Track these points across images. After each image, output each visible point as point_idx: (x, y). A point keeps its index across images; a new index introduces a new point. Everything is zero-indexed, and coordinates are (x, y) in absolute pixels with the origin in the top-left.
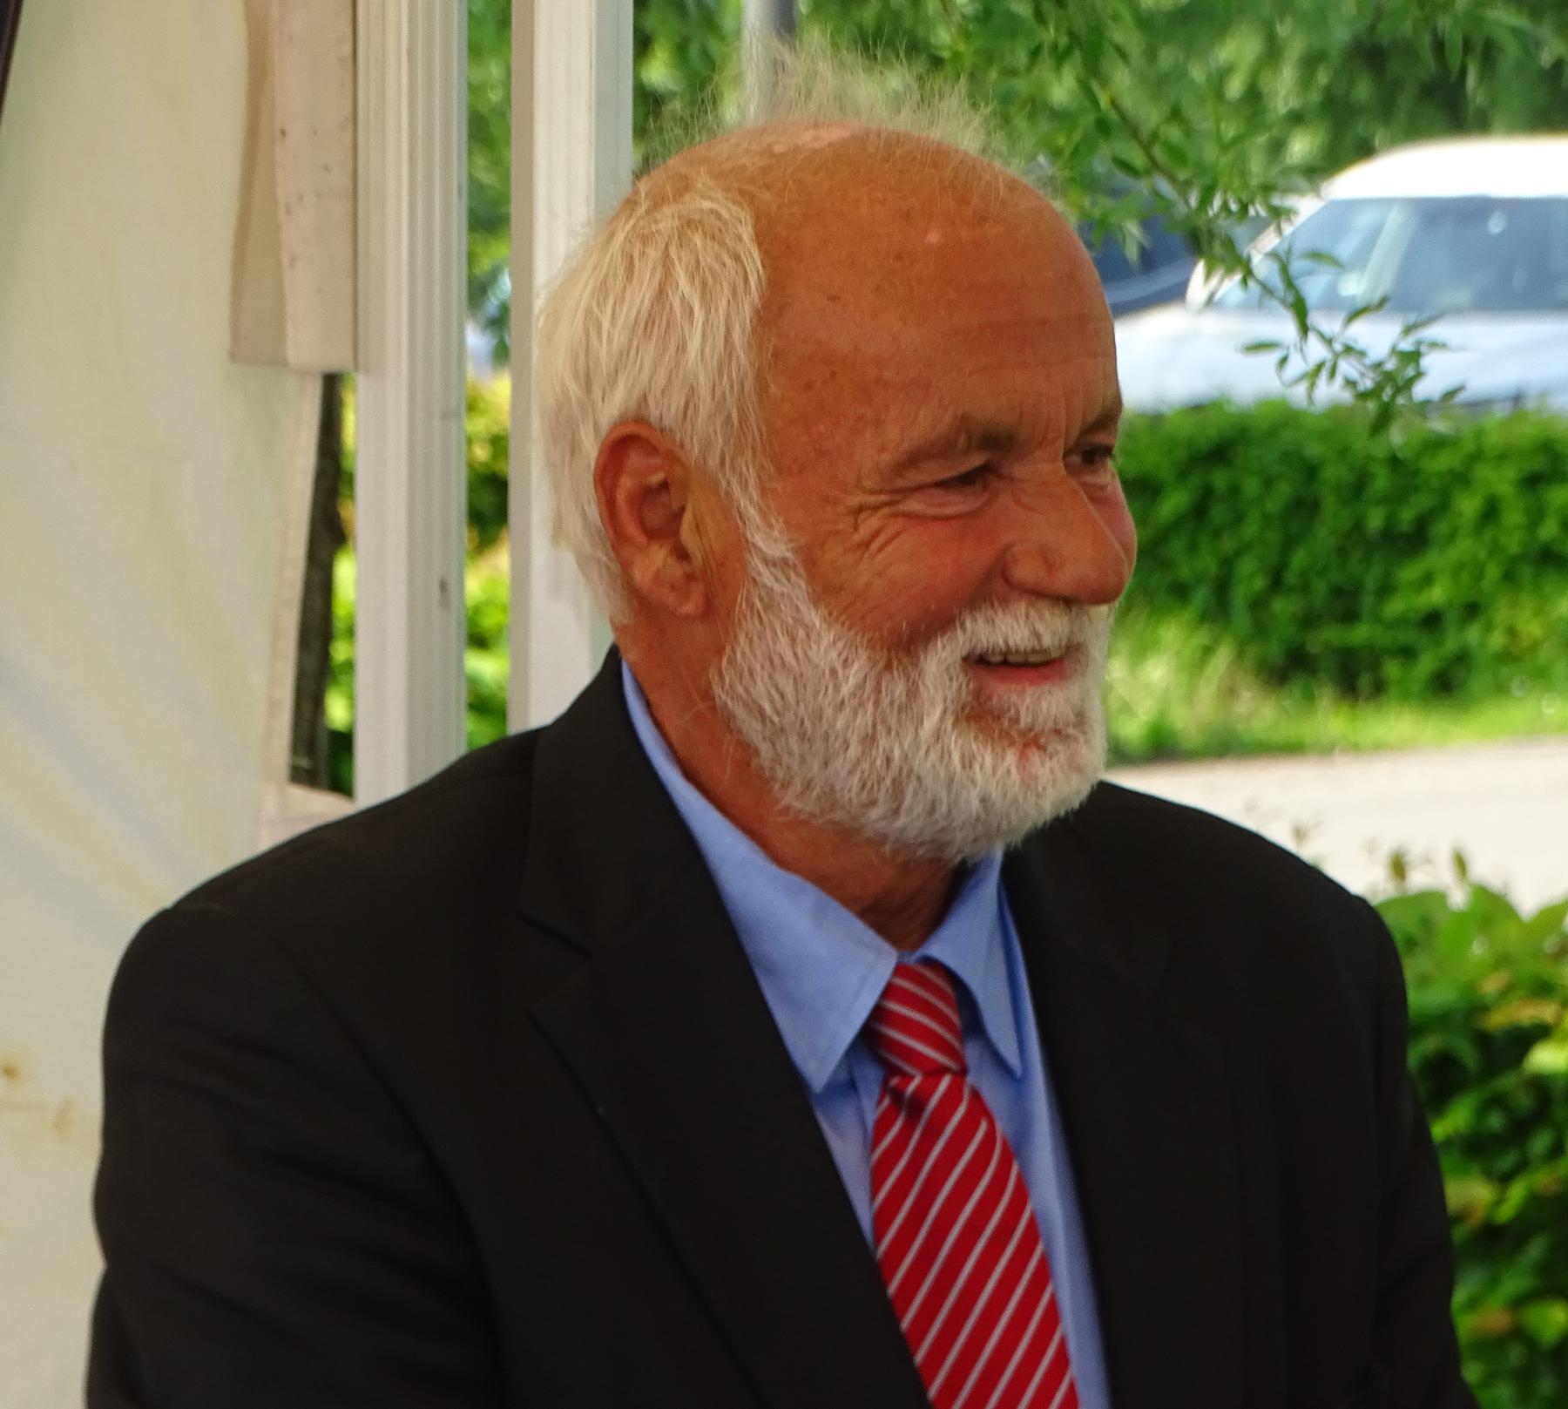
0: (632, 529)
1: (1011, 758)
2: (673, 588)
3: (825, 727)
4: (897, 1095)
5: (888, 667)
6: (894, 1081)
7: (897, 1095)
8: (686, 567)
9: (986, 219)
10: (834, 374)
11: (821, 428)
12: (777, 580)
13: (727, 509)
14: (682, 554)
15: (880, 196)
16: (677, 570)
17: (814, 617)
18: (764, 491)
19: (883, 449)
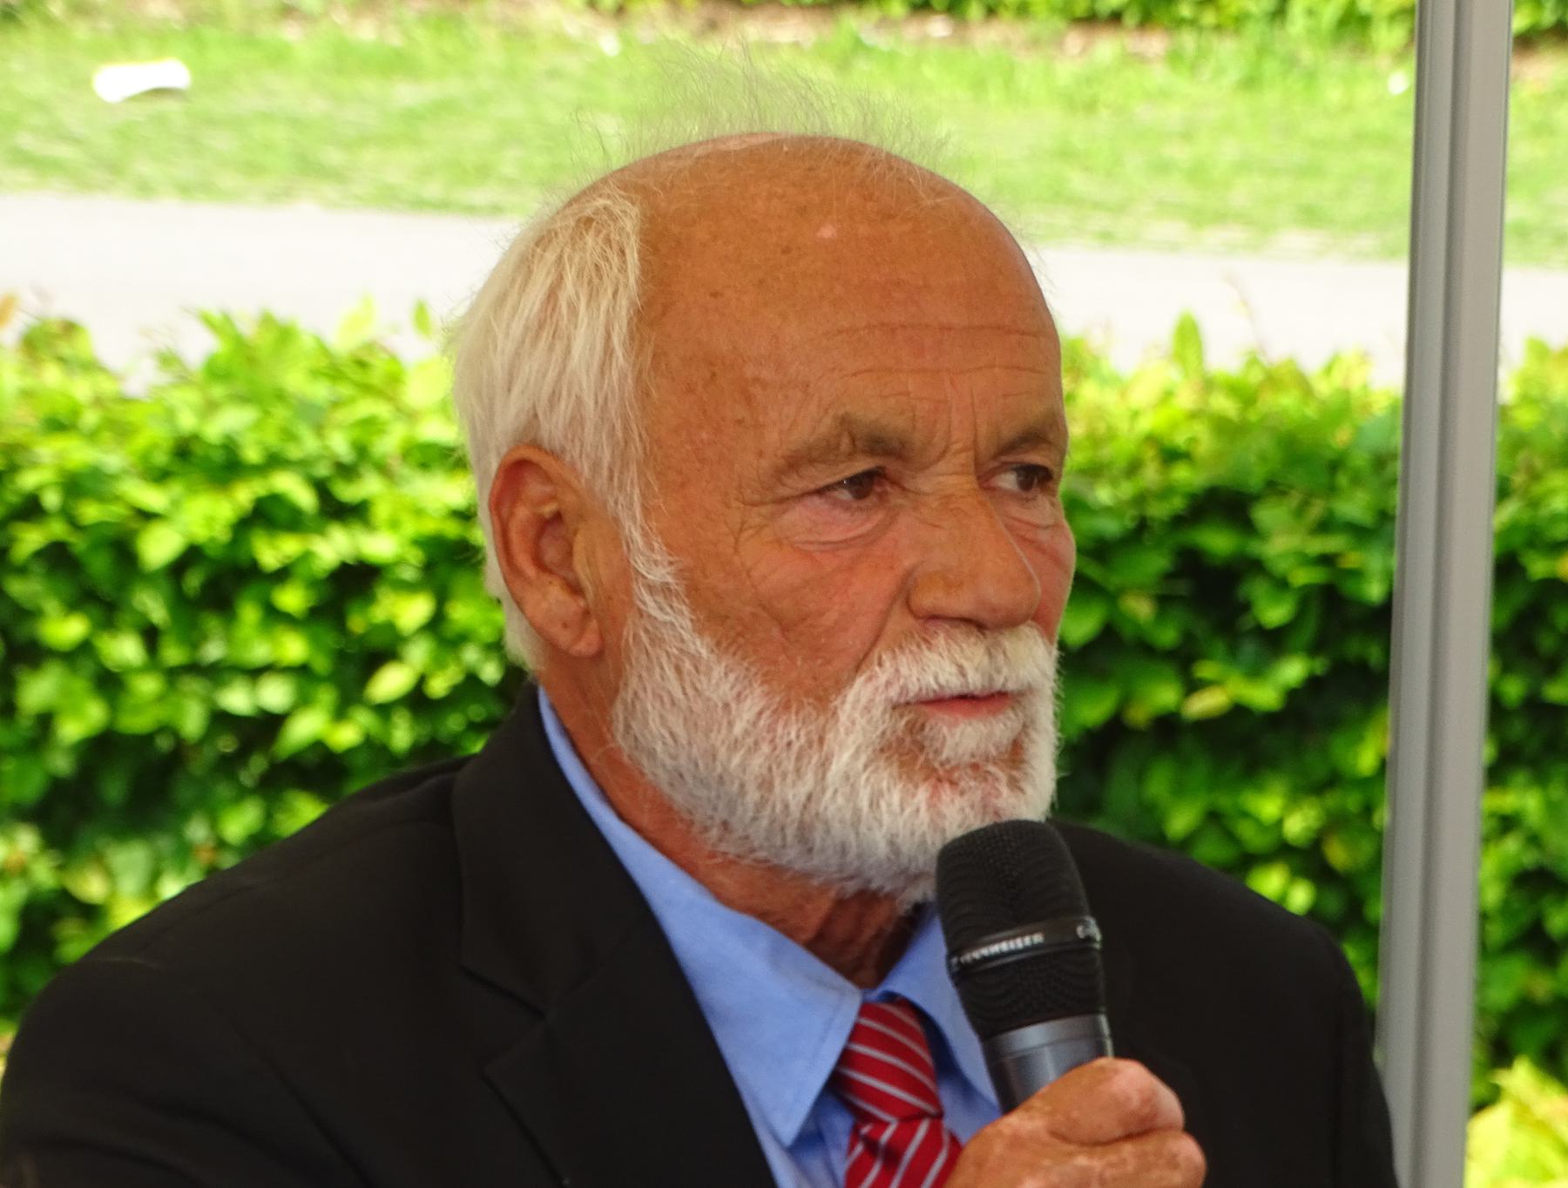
0: (524, 561)
1: (922, 794)
2: (565, 625)
3: (719, 769)
4: (872, 1145)
5: (786, 706)
6: (866, 1130)
7: (872, 1145)
8: (582, 603)
9: (891, 217)
10: (714, 374)
11: (704, 436)
12: (661, 609)
13: (616, 538)
14: (575, 589)
15: (780, 191)
16: (573, 606)
17: (700, 647)
18: (646, 510)
19: (761, 454)
